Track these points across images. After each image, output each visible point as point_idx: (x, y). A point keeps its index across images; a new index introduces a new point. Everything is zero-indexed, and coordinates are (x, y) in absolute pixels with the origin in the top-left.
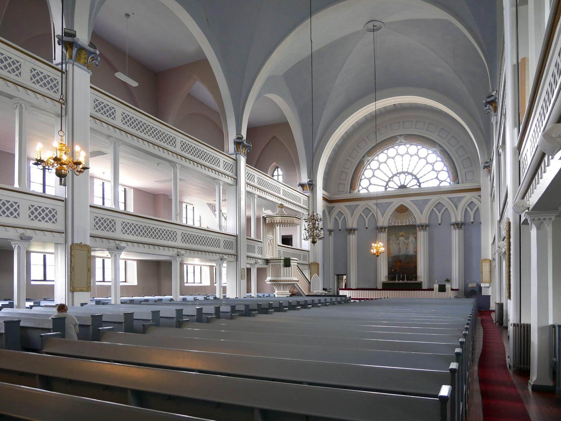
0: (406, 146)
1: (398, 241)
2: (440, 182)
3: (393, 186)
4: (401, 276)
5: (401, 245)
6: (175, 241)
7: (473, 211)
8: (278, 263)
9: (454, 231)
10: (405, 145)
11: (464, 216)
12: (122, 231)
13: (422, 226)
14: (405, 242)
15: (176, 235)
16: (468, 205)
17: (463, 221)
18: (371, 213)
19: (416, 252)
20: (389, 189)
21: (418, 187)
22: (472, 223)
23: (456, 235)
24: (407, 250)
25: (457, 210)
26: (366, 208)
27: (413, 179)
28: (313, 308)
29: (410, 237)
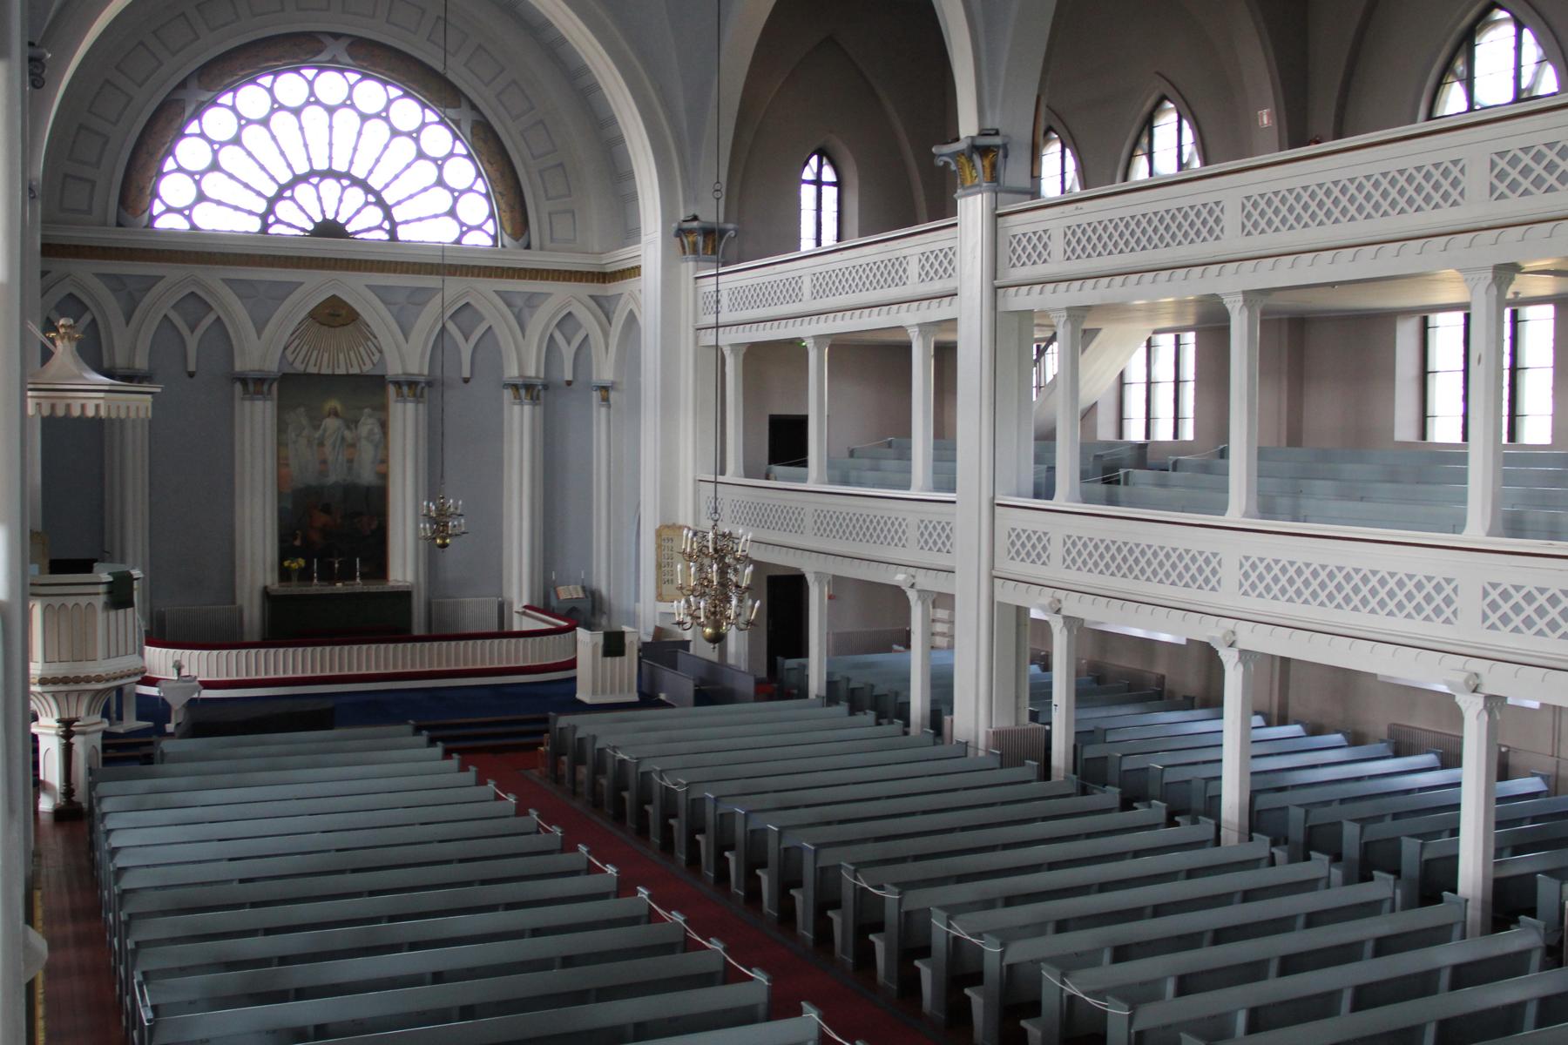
0: (344, 77)
1: (318, 434)
2: (465, 229)
3: (294, 219)
4: (337, 565)
5: (328, 449)
7: (572, 344)
8: (83, 601)
9: (516, 408)
10: (214, 103)
11: (547, 357)
13: (412, 384)
14: (343, 439)
15: (1243, 580)
16: (559, 325)
17: (426, 372)
18: (211, 318)
19: (384, 476)
20: (273, 230)
21: (385, 237)
22: (569, 383)
23: (520, 420)
24: (350, 469)
25: (524, 336)
26: (71, 295)
27: (367, 203)
29: (363, 420)
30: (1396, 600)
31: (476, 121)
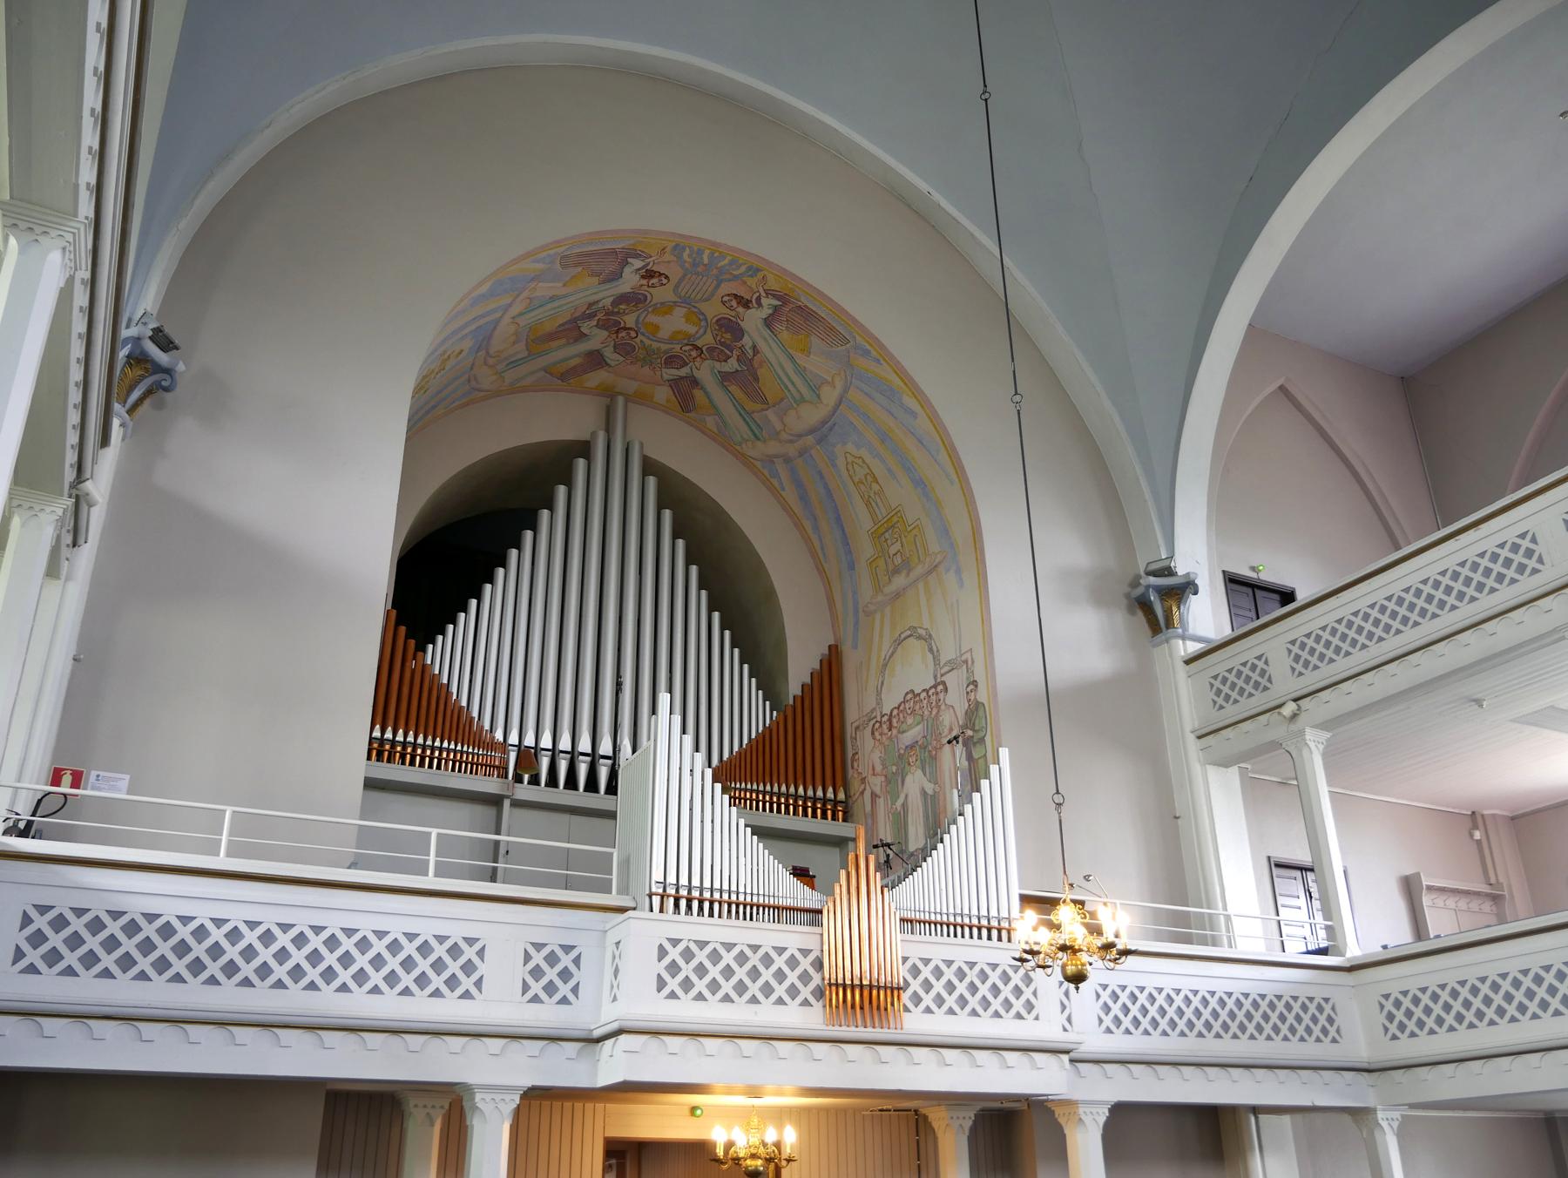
6: (1334, 1041)
12: (1386, 1030)
28: (965, 814)
30: (1523, 989)
31: (818, 985)
